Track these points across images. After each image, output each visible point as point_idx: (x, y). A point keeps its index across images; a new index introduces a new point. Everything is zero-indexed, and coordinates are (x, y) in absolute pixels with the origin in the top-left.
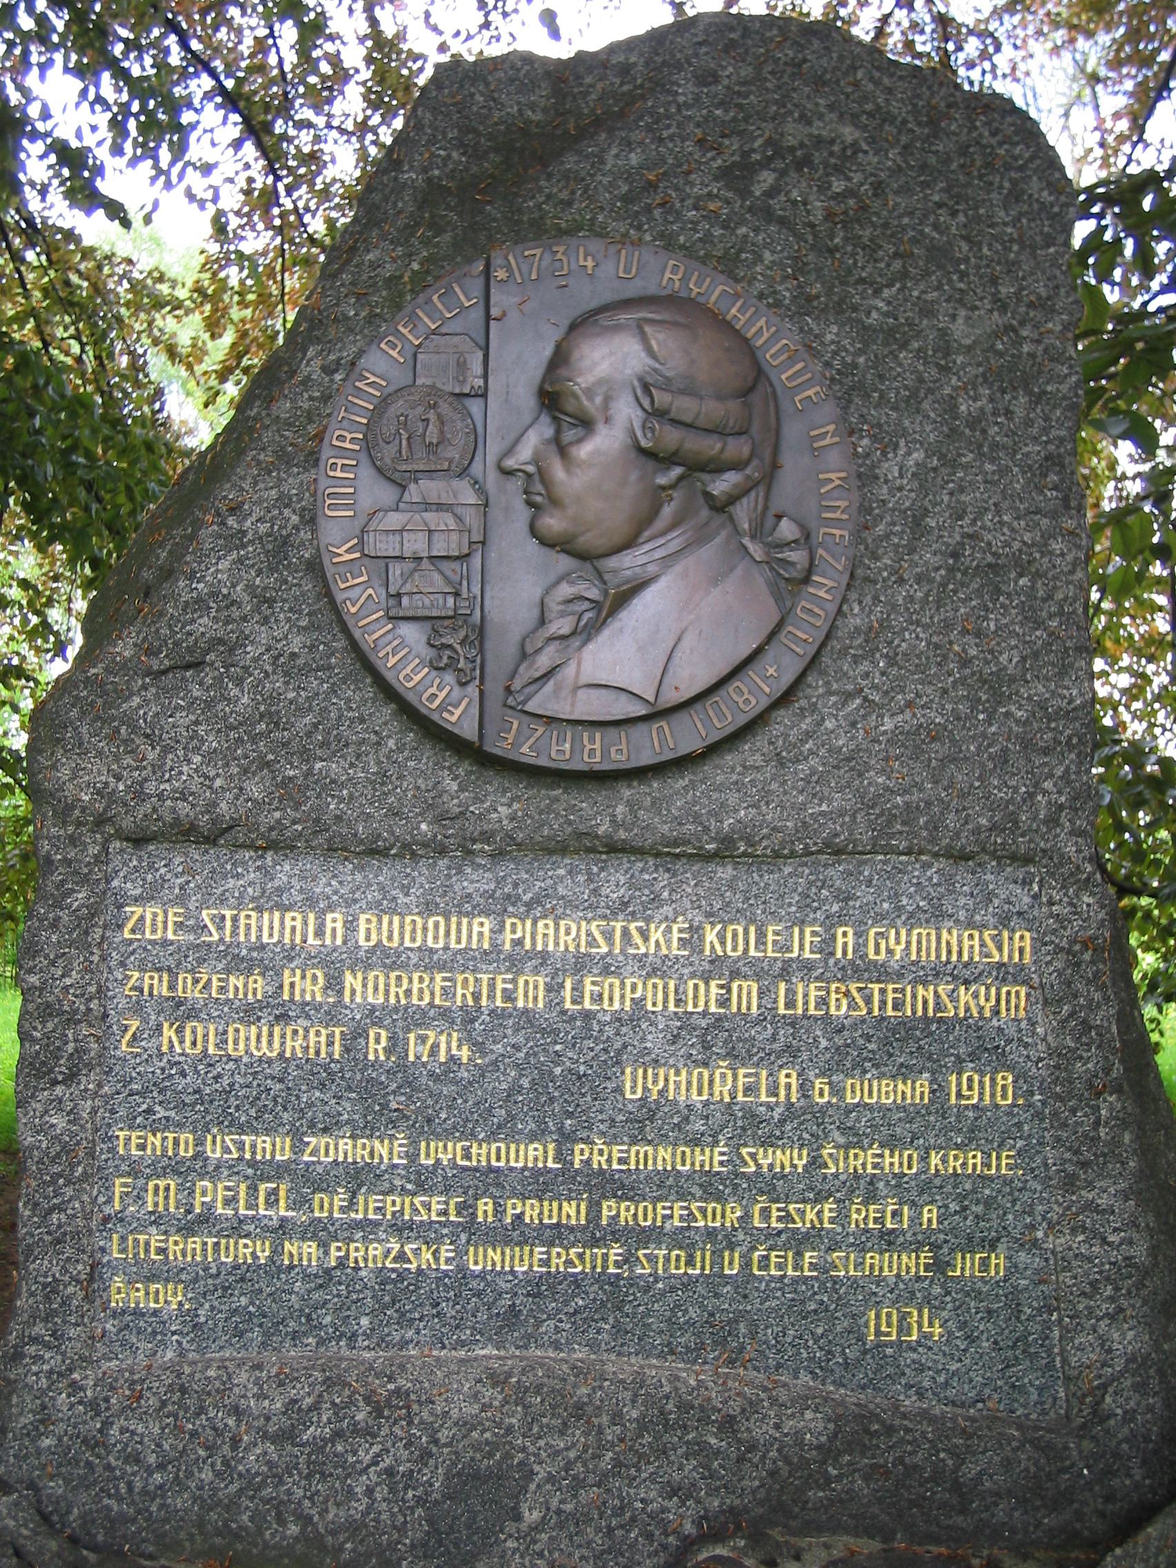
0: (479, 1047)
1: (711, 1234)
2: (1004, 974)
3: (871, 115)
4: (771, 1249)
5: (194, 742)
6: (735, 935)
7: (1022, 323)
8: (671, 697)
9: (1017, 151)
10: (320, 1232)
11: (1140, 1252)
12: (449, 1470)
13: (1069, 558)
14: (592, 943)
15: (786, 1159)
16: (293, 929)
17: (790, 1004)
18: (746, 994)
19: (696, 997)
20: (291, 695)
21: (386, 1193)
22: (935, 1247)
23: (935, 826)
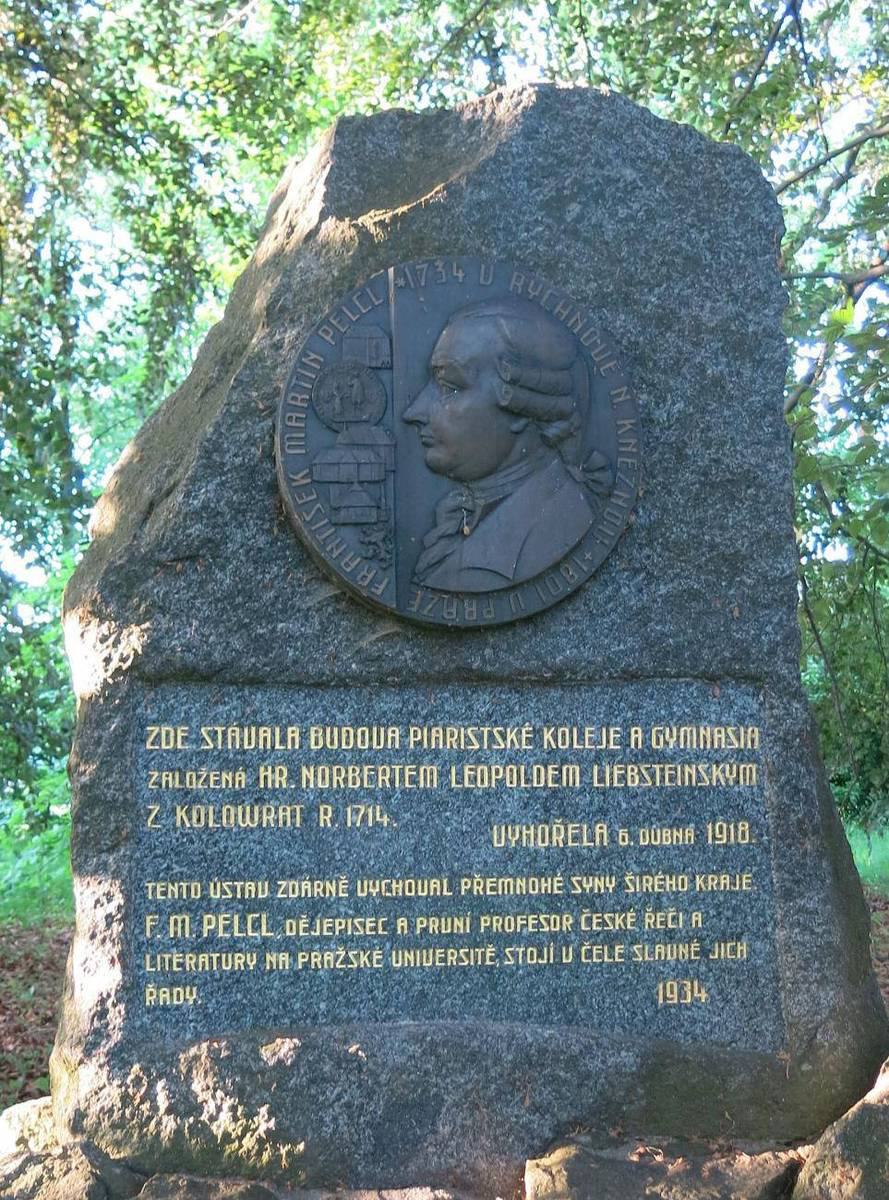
0: (395, 816)
1: (553, 936)
2: (741, 756)
3: (643, 160)
4: (594, 944)
6: (564, 734)
7: (748, 310)
9: (744, 185)
10: (290, 946)
11: (836, 939)
12: (388, 1101)
13: (781, 474)
14: (469, 742)
16: (265, 739)
17: (601, 780)
18: (572, 774)
19: (539, 776)
20: (260, 577)
21: (334, 918)
22: (701, 940)
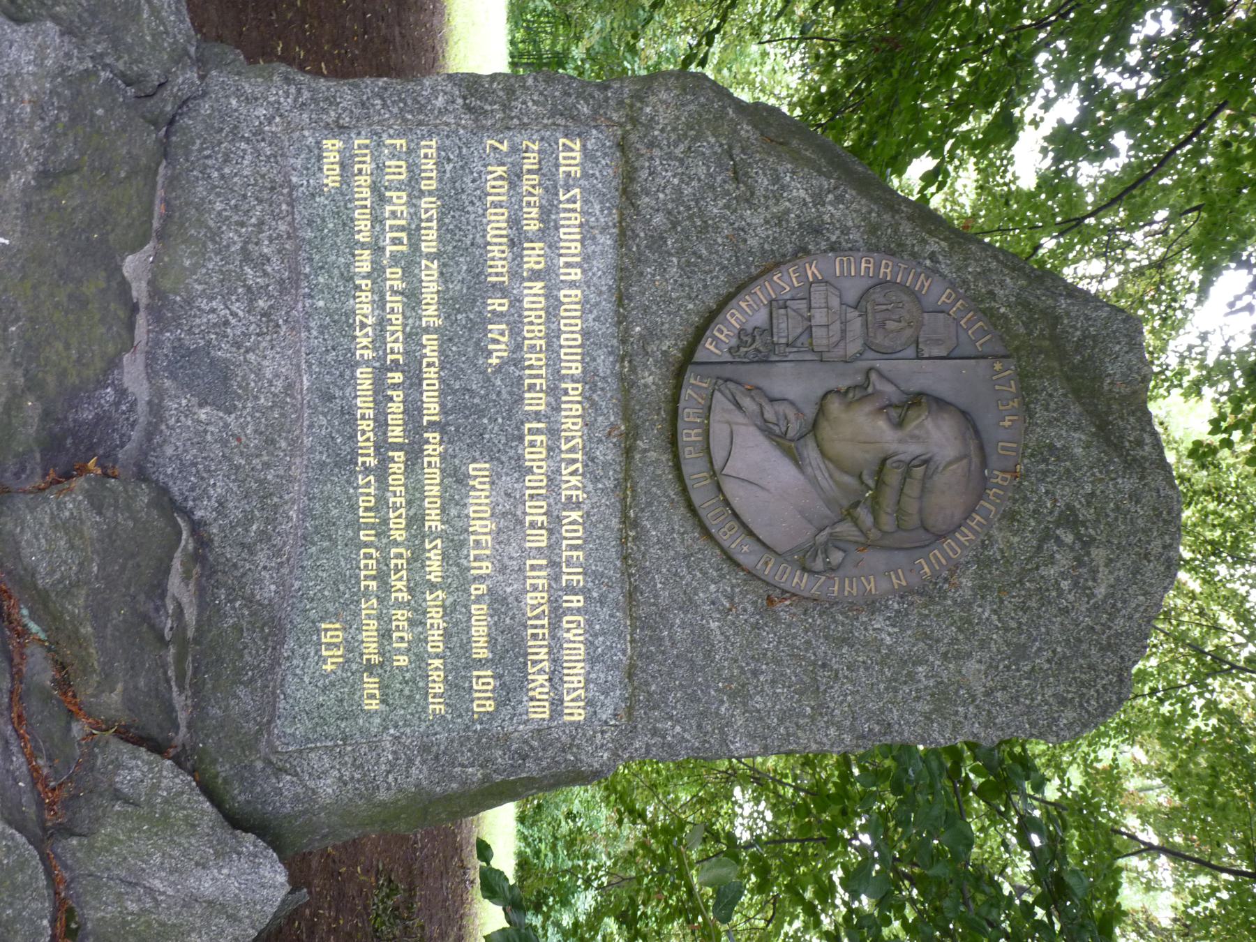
1: (385, 522)
2: (557, 704)
5: (687, 179)
8: (730, 487)
10: (377, 273)
11: (382, 795)
15: (434, 569)
23: (649, 657)
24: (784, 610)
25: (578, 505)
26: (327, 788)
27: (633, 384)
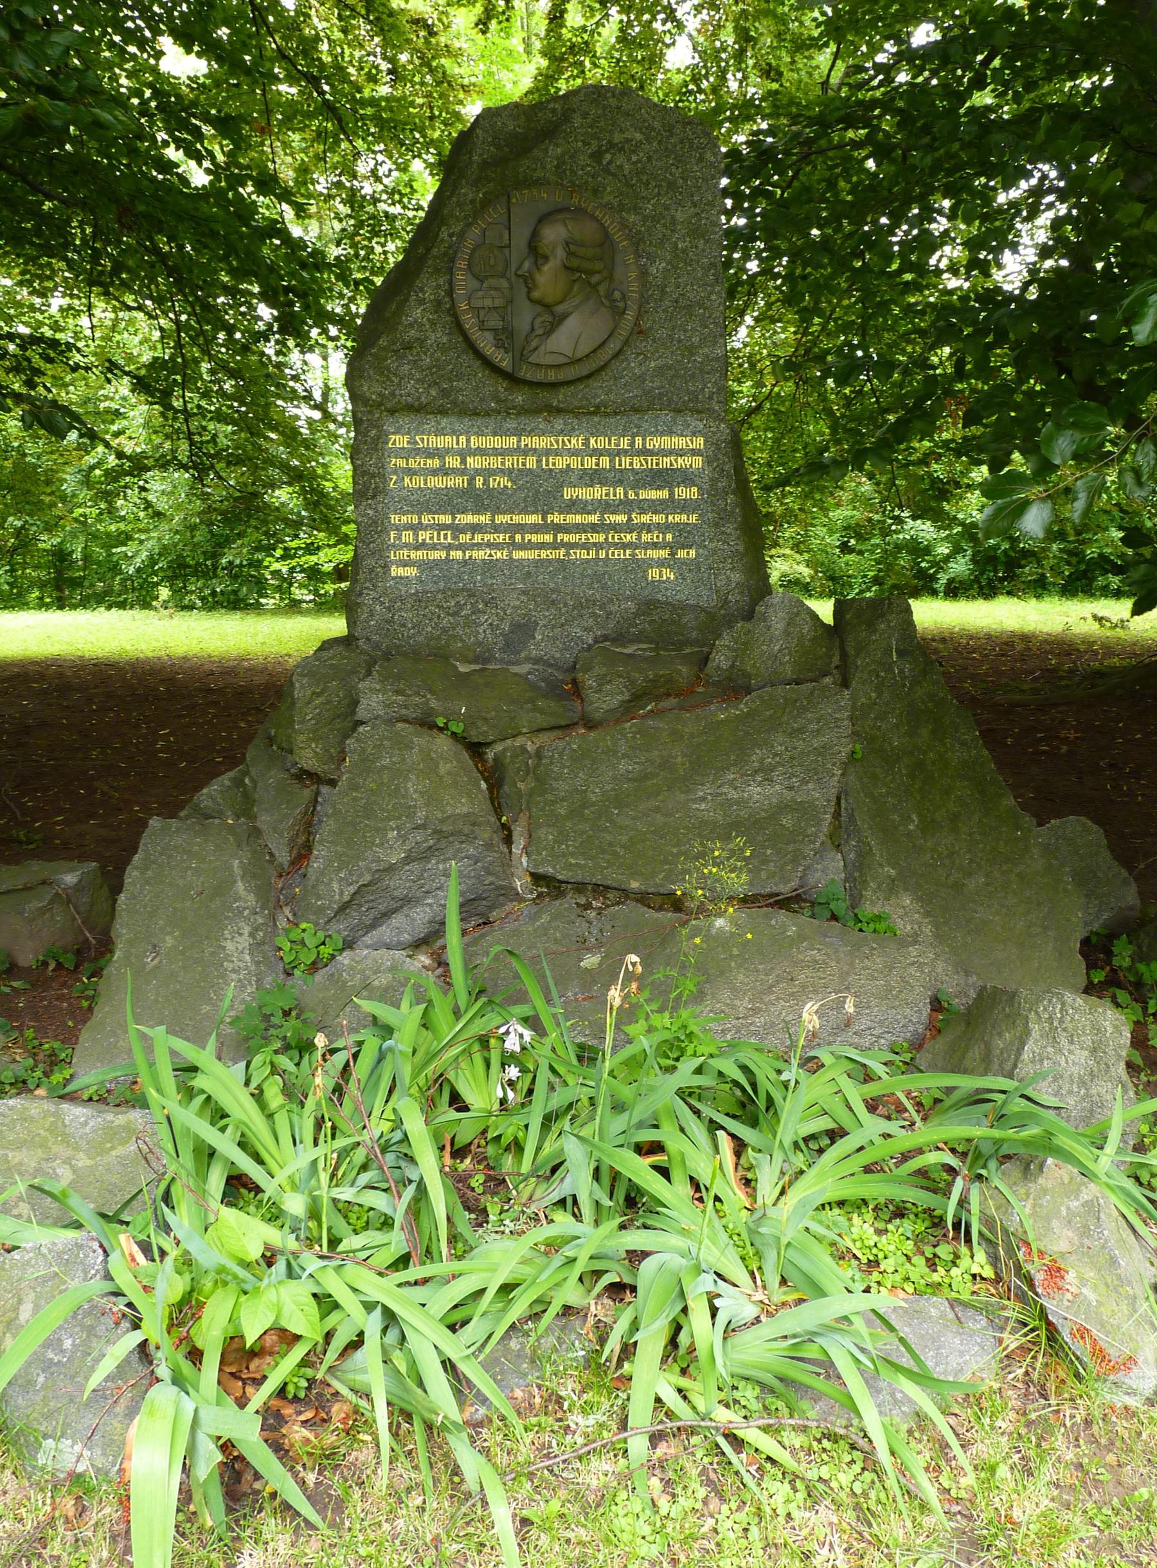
1: (595, 544)
2: (694, 452)
5: (411, 376)
8: (579, 355)
10: (462, 547)
11: (741, 548)
15: (621, 518)
18: (605, 462)
23: (670, 401)
24: (646, 324)
25: (587, 440)
26: (736, 577)
27: (522, 408)
